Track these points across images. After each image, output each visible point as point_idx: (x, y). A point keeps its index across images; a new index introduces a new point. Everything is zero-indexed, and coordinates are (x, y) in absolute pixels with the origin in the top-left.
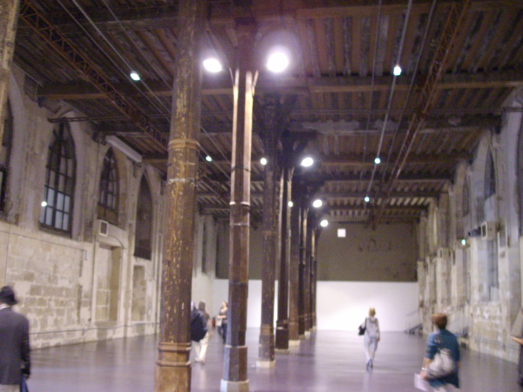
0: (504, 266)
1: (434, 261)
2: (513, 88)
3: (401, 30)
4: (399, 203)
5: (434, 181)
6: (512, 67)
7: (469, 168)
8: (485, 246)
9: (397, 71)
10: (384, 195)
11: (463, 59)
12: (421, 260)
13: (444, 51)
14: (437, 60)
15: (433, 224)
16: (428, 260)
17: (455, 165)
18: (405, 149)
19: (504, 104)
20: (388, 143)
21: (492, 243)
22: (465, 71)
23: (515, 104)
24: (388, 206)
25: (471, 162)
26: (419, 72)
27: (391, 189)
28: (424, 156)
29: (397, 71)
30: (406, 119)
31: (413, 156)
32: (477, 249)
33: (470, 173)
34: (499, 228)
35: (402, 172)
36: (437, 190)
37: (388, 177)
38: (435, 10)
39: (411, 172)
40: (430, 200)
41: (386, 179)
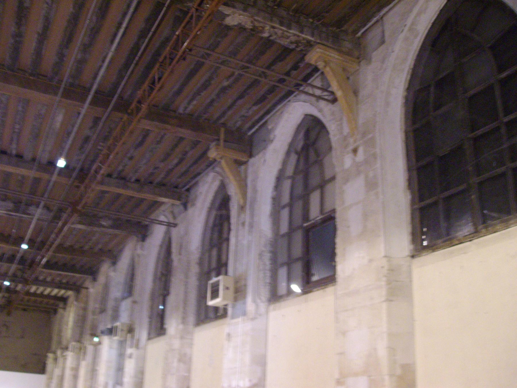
0: (130, 366)
1: (64, 354)
2: (163, 203)
3: (73, 126)
4: (39, 292)
5: (77, 275)
6: (164, 185)
7: (112, 268)
8: (115, 345)
9: (61, 163)
10: (26, 282)
11: (125, 166)
12: (51, 352)
13: (108, 156)
14: (101, 162)
15: (69, 317)
16: (59, 352)
17: (100, 262)
18: (55, 240)
19: (153, 216)
20: (38, 231)
21: (122, 344)
22: (124, 178)
23: (162, 218)
24: (28, 293)
25: (114, 263)
26: (81, 170)
27: (34, 276)
28: (71, 250)
29: (61, 163)
30: (61, 210)
31: (61, 248)
32: (107, 347)
33: (112, 274)
34: (131, 330)
35: (48, 262)
36: (78, 284)
37: (32, 264)
38: (108, 117)
39: (56, 263)
40: (70, 293)
41: (31, 266)
